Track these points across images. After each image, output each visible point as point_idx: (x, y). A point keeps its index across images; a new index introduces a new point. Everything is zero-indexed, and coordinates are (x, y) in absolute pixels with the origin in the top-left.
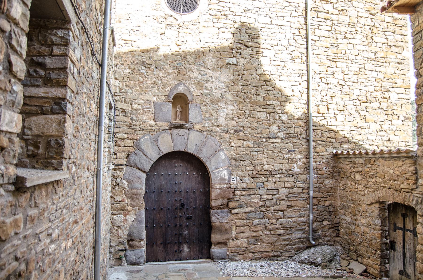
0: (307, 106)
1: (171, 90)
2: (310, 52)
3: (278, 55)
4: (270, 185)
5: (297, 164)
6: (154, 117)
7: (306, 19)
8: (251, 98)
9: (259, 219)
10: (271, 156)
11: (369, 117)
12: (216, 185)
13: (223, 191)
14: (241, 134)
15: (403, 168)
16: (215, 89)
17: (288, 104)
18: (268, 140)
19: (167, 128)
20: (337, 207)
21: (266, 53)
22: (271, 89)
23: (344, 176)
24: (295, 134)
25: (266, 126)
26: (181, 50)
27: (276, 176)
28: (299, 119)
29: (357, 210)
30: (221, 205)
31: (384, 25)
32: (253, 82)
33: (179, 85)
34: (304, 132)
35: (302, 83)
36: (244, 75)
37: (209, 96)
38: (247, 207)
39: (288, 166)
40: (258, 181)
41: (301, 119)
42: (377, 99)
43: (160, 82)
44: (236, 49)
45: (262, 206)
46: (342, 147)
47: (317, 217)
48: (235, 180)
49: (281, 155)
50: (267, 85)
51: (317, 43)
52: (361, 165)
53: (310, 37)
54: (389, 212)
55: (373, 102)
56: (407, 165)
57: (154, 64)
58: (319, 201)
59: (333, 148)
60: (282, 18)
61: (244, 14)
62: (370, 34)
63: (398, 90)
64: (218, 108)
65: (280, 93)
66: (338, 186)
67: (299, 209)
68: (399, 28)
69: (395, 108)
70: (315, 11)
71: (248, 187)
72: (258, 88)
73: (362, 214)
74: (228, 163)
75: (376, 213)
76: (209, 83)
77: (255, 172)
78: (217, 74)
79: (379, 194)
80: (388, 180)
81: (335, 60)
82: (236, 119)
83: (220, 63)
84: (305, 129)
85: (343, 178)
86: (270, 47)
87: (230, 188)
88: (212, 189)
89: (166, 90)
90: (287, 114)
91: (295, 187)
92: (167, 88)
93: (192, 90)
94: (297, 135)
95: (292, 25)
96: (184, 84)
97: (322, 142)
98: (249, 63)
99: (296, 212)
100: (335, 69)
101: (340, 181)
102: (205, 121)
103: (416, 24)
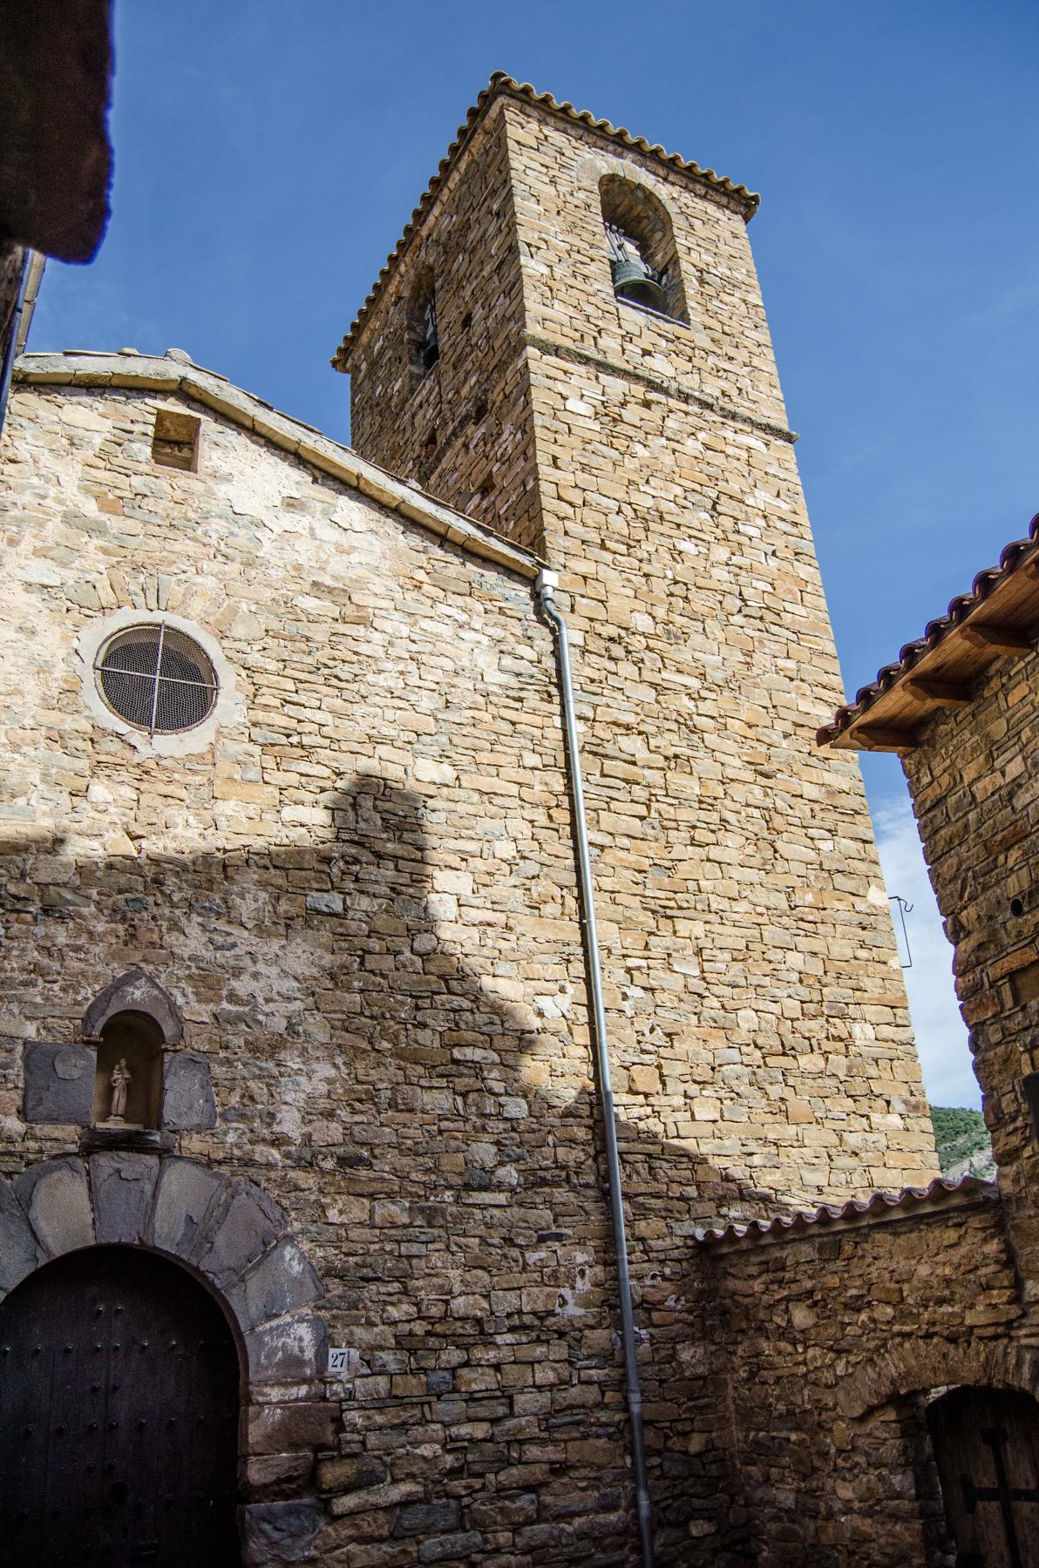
0: (591, 1069)
1: (98, 999)
2: (590, 883)
3: (483, 891)
4: (479, 1381)
5: (573, 1288)
6: (19, 1103)
7: (569, 776)
8: (397, 1037)
9: (444, 1532)
10: (477, 1258)
11: (797, 1104)
12: (267, 1390)
13: (295, 1412)
14: (363, 1173)
15: (963, 1250)
16: (267, 1000)
17: (527, 1060)
18: (463, 1194)
19: (72, 1148)
20: (732, 1456)
21: (442, 879)
22: (466, 1004)
23: (744, 1325)
24: (557, 1172)
25: (453, 1143)
26: (143, 855)
27: (499, 1339)
28: (568, 1113)
29: (813, 1450)
30: (290, 1479)
31: (803, 809)
32: (404, 979)
33: (129, 979)
34: (590, 1162)
35: (570, 988)
36: (370, 953)
37: (243, 1026)
38: (395, 1481)
39: (542, 1297)
40: (431, 1363)
41: (575, 1117)
42: (814, 1041)
43: (56, 966)
44: (341, 863)
45: (454, 1473)
46: (724, 1216)
47: (664, 1504)
48: (341, 1361)
49: (515, 1253)
50: (450, 992)
51: (608, 857)
52: (805, 1267)
53: (587, 835)
54: (935, 1439)
55: (803, 1053)
56: (973, 1239)
57: (37, 899)
58: (667, 1437)
59: (695, 1219)
60: (493, 770)
61: (368, 749)
62: (765, 834)
63: (871, 1011)
64: (275, 1071)
65: (496, 1019)
66: (724, 1369)
67: (592, 1474)
68: (846, 818)
69: (872, 1071)
70: (595, 754)
71: (395, 1392)
72: (420, 1002)
73: (840, 1462)
74: (313, 1293)
75: (892, 1448)
76: (245, 977)
77: (419, 1328)
78: (275, 945)
79: (892, 1366)
80: (917, 1305)
81: (669, 912)
82: (343, 1114)
83: (283, 907)
84: (591, 1151)
85: (742, 1331)
86: (456, 862)
87: (324, 1399)
88: (252, 1409)
89: (79, 998)
90: (525, 1097)
91: (575, 1381)
92: (83, 992)
93: (180, 1001)
94: (563, 1174)
95: (525, 793)
96: (151, 980)
97: (653, 1201)
98: (386, 911)
99: (583, 1489)
100: (669, 941)
101: (731, 1348)
102: (226, 1120)
103: (926, 780)
